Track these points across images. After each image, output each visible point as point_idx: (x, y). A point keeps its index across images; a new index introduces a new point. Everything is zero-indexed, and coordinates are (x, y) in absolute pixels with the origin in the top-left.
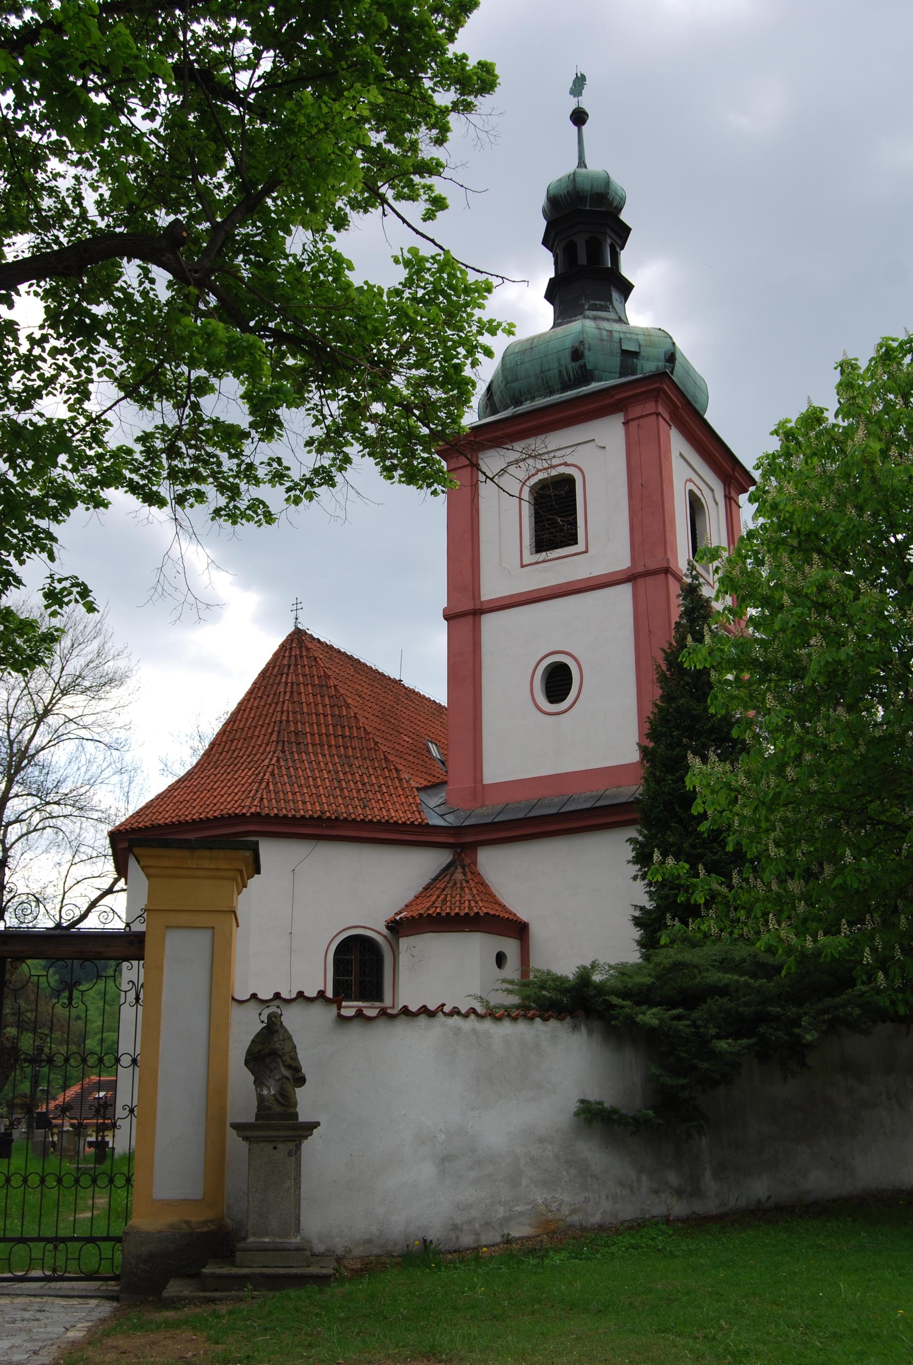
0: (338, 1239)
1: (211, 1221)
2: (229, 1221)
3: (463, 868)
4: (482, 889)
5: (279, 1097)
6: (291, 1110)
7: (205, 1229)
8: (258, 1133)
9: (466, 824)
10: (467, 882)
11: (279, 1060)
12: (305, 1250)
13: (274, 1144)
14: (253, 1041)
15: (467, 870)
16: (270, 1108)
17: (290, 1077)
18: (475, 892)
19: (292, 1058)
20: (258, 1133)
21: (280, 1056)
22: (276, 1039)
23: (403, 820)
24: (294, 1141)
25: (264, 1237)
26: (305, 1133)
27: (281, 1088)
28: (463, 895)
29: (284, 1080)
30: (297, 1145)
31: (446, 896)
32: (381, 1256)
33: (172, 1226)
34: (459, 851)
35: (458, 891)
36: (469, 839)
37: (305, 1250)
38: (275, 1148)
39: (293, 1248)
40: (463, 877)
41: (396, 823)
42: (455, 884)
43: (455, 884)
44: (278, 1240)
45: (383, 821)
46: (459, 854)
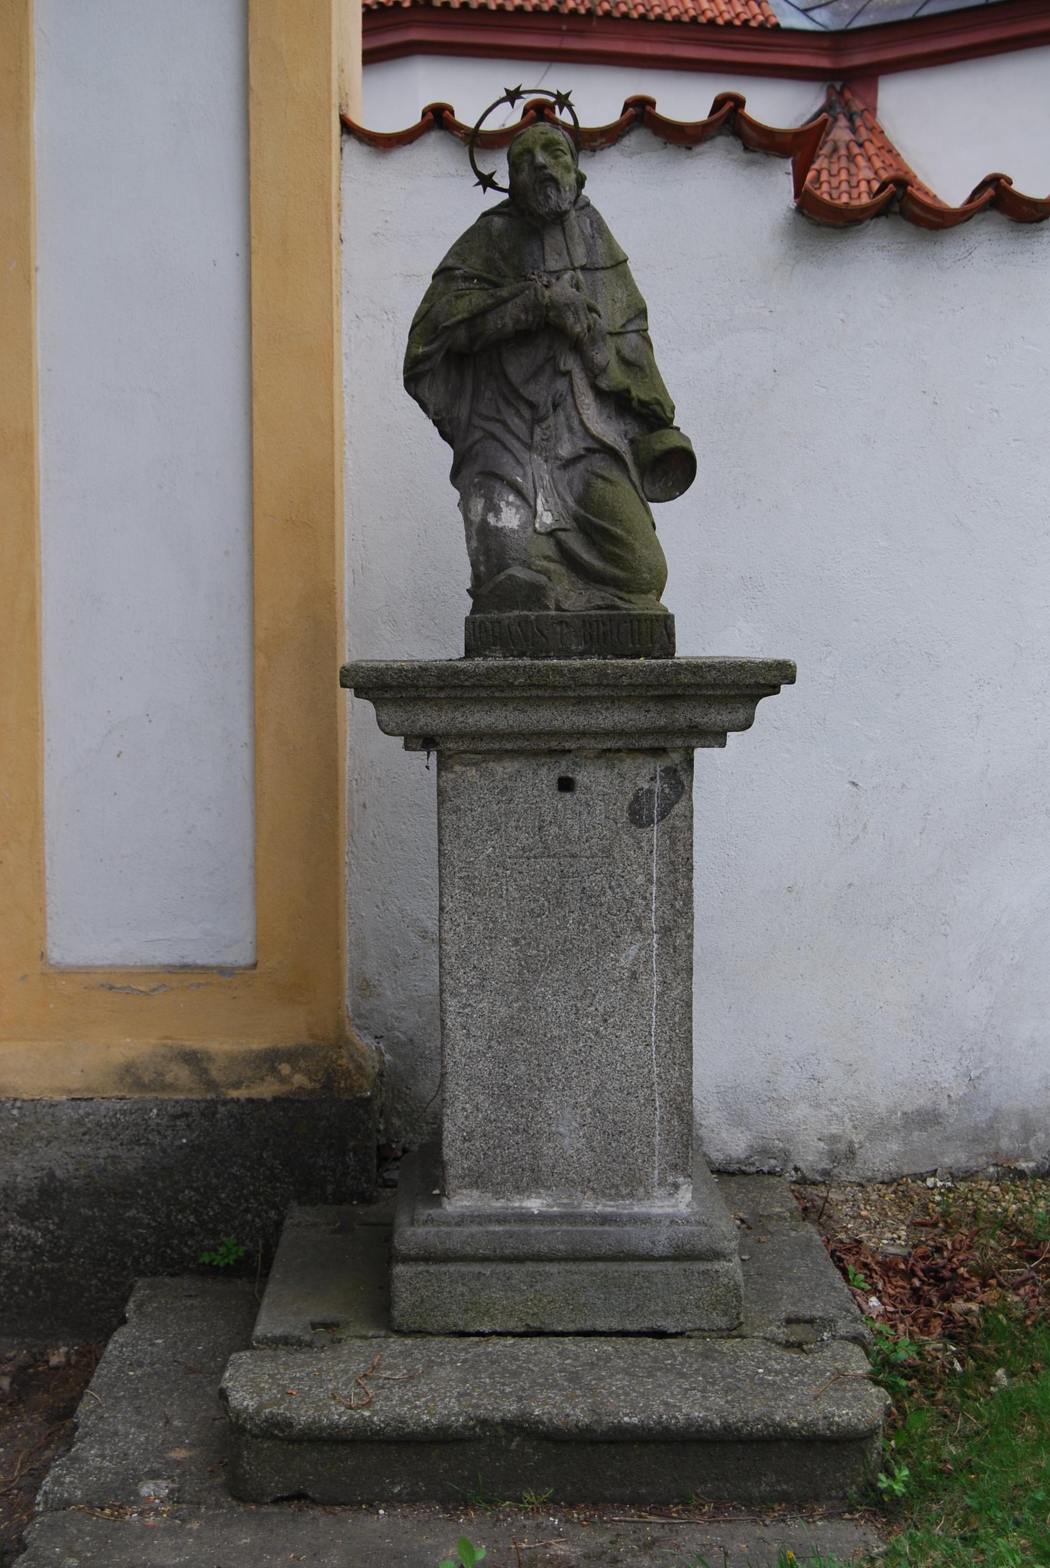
0: (802, 1110)
1: (291, 1056)
2: (365, 1043)
3: (851, 119)
4: (889, 160)
5: (575, 543)
6: (639, 606)
7: (266, 1090)
8: (479, 718)
9: (858, 23)
10: (861, 145)
11: (570, 363)
12: (717, 1255)
13: (563, 768)
14: (443, 273)
15: (858, 122)
16: (535, 594)
17: (622, 446)
18: (878, 164)
19: (627, 363)
20: (479, 718)
21: (577, 347)
22: (553, 264)
23: (727, 16)
24: (658, 752)
25: (520, 1190)
26: (716, 717)
27: (584, 500)
28: (853, 170)
29: (600, 464)
30: (670, 772)
31: (819, 172)
32: (969, 1175)
33: (129, 1074)
34: (838, 86)
35: (844, 162)
36: (860, 59)
37: (717, 1255)
38: (566, 785)
39: (662, 1240)
40: (852, 137)
41: (712, 22)
42: (835, 150)
43: (835, 150)
44: (590, 1205)
45: (685, 18)
46: (841, 94)
